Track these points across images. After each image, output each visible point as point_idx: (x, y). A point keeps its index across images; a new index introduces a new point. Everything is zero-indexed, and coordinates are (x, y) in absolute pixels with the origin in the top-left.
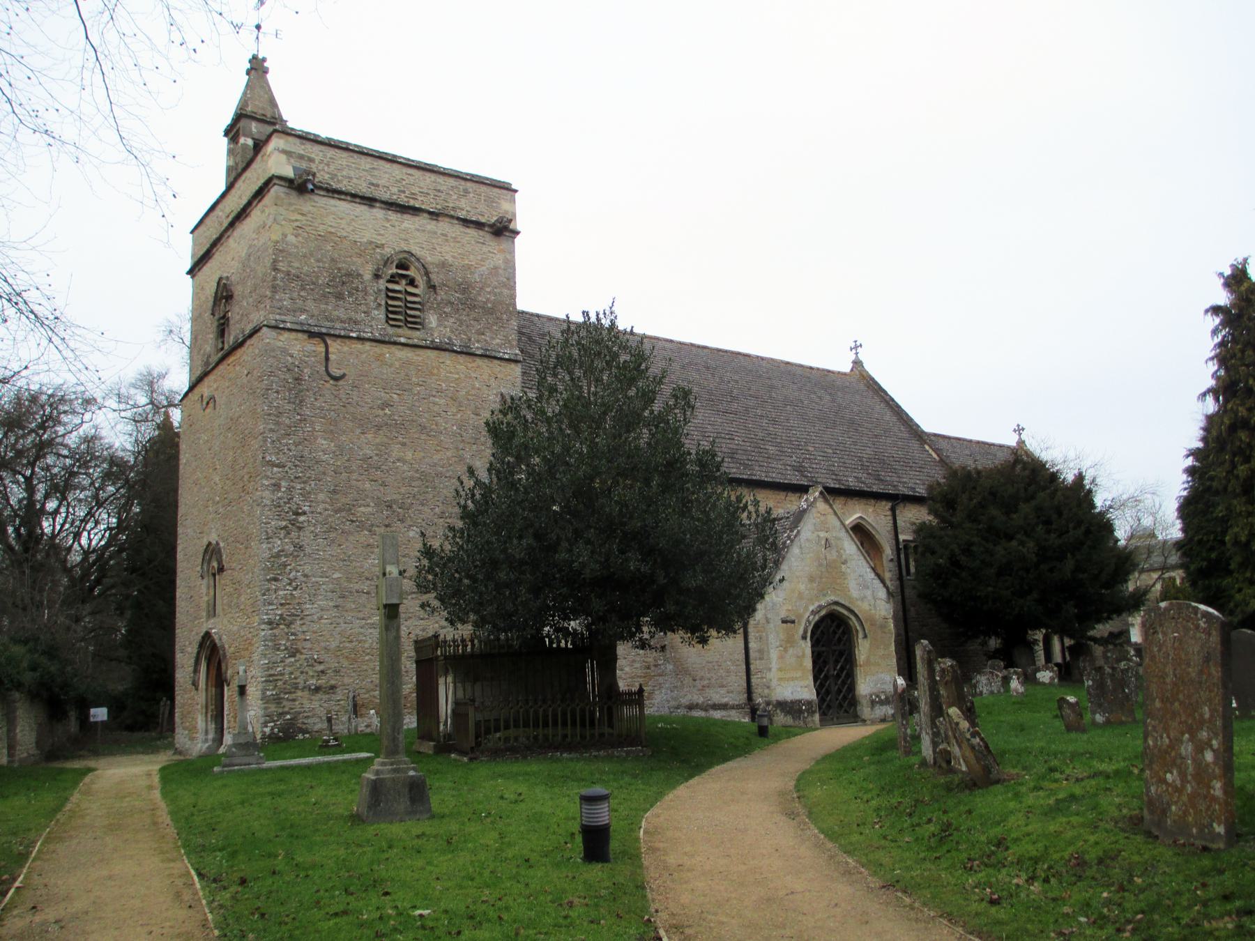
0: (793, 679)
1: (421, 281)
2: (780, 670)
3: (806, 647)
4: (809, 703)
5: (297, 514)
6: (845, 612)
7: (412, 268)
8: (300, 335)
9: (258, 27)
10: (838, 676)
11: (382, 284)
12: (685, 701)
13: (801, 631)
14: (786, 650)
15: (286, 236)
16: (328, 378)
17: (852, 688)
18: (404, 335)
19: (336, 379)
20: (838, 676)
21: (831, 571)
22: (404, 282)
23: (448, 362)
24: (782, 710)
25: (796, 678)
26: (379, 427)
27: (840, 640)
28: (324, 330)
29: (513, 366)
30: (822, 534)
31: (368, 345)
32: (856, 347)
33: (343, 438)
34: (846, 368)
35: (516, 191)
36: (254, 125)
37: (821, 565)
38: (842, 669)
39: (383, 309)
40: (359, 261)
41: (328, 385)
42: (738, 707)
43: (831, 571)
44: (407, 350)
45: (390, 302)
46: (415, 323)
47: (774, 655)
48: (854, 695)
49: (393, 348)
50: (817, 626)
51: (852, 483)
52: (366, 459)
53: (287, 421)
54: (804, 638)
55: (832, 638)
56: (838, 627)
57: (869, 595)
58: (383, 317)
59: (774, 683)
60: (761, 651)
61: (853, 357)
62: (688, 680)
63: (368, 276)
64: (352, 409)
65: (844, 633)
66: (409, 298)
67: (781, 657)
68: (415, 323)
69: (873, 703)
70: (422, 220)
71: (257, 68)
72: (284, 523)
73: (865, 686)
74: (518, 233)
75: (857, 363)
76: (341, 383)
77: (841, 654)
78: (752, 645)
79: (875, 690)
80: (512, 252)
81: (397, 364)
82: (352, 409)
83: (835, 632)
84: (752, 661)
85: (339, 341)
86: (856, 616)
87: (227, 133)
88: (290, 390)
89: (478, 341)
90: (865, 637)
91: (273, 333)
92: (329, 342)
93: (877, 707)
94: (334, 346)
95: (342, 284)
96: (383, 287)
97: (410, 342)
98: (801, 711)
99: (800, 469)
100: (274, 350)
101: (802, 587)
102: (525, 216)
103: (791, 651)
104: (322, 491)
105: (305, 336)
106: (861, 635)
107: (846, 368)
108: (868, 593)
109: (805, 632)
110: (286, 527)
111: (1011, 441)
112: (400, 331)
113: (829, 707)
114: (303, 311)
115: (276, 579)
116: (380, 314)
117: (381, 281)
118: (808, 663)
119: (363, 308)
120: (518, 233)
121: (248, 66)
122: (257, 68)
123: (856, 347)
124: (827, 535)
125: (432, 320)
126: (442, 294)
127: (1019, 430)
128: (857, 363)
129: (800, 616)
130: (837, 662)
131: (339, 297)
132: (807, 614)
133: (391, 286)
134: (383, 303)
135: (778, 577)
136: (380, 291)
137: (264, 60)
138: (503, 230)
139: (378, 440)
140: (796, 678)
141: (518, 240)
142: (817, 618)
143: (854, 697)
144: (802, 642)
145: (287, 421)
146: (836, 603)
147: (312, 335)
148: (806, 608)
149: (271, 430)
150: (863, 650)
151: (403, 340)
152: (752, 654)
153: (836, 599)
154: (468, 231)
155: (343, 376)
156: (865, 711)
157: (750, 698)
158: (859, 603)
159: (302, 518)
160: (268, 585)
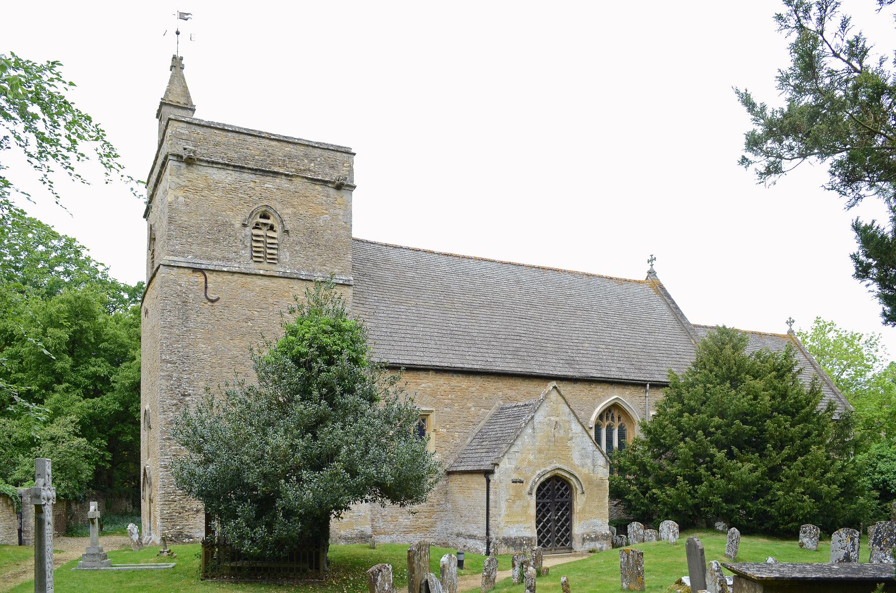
0: (518, 522)
1: (278, 227)
2: (508, 516)
3: (533, 500)
4: (530, 539)
5: (184, 395)
6: (568, 476)
7: (272, 218)
8: (186, 270)
9: (178, 33)
10: (559, 520)
11: (248, 231)
12: (456, 531)
13: (528, 489)
14: (514, 502)
15: (178, 198)
16: (206, 301)
17: (569, 529)
18: (262, 268)
19: (212, 301)
20: (559, 520)
21: (558, 444)
22: (265, 229)
23: (296, 287)
24: (506, 544)
25: (521, 522)
26: (243, 335)
27: (562, 495)
28: (203, 267)
29: (346, 288)
30: (552, 418)
31: (236, 277)
32: (652, 260)
33: (218, 343)
34: (642, 277)
35: (354, 154)
36: (175, 107)
37: (550, 441)
38: (563, 515)
39: (249, 249)
40: (231, 214)
41: (206, 306)
42: (481, 539)
43: (559, 444)
44: (265, 279)
45: (254, 244)
46: (274, 260)
47: (503, 505)
48: (571, 534)
49: (255, 278)
50: (543, 484)
51: (614, 374)
52: (234, 358)
53: (177, 332)
54: (530, 494)
55: (555, 496)
56: (562, 485)
57: (590, 467)
58: (248, 255)
59: (502, 524)
60: (496, 502)
61: (648, 268)
62: (458, 516)
63: (238, 225)
64: (224, 323)
65: (566, 489)
66: (269, 241)
67: (510, 507)
68: (274, 260)
69: (584, 539)
70: (282, 182)
71: (177, 64)
72: (175, 402)
73: (578, 529)
74: (355, 187)
75: (651, 273)
76: (216, 304)
77: (562, 505)
78: (491, 497)
79: (588, 531)
80: (350, 201)
81: (258, 289)
82: (224, 323)
83: (559, 489)
84: (490, 508)
85: (214, 274)
86: (576, 477)
87: (157, 117)
88: (179, 310)
89: (320, 271)
90: (583, 493)
91: (167, 270)
92: (207, 275)
93: (587, 543)
94: (211, 277)
95: (219, 231)
96: (249, 233)
97: (268, 273)
98: (521, 544)
99: (570, 362)
100: (167, 282)
101: (531, 457)
102: (362, 173)
103: (518, 502)
104: (202, 380)
105: (190, 271)
106: (579, 492)
107: (642, 277)
108: (589, 462)
109: (531, 489)
110: (176, 405)
111: (783, 330)
112: (260, 265)
113: (548, 542)
114: (189, 252)
115: (169, 439)
116: (246, 253)
117: (247, 229)
118: (533, 511)
119: (234, 249)
120: (355, 187)
121: (183, 62)
122: (177, 64)
123: (652, 260)
124: (557, 419)
125: (285, 256)
126: (293, 237)
127: (790, 322)
128: (651, 273)
129: (527, 478)
130: (558, 510)
131: (216, 241)
132: (534, 478)
133: (256, 232)
134: (249, 245)
135: (723, 392)
136: (246, 236)
137: (181, 59)
138: (343, 186)
139: (242, 345)
140: (521, 522)
141: (354, 192)
142: (542, 479)
143: (570, 535)
144: (529, 497)
145: (177, 332)
146: (559, 469)
147: (195, 270)
148: (534, 471)
149: (166, 338)
150: (579, 502)
151: (262, 272)
152: (491, 504)
153: (558, 465)
154: (317, 187)
155: (218, 299)
156: (577, 545)
157: (488, 534)
158: (580, 468)
159: (187, 398)
160: (164, 443)
